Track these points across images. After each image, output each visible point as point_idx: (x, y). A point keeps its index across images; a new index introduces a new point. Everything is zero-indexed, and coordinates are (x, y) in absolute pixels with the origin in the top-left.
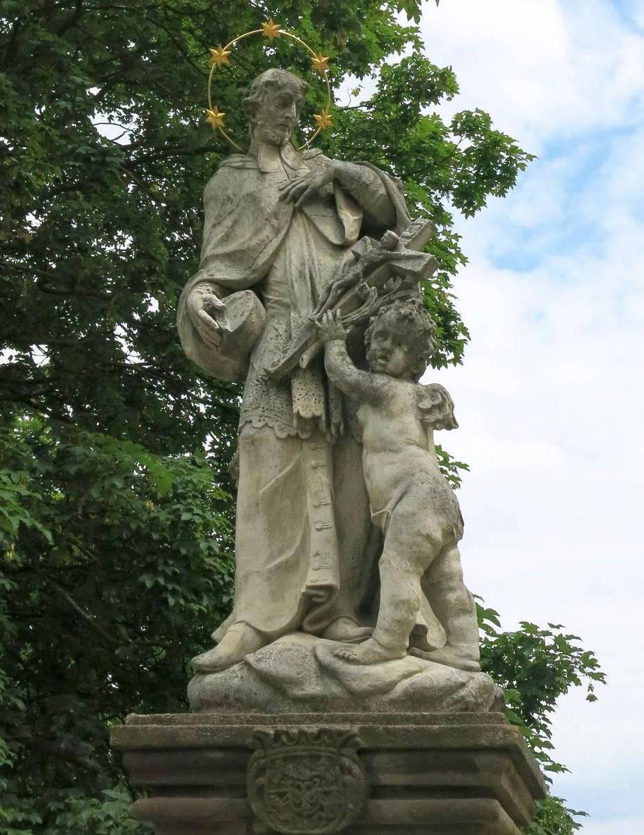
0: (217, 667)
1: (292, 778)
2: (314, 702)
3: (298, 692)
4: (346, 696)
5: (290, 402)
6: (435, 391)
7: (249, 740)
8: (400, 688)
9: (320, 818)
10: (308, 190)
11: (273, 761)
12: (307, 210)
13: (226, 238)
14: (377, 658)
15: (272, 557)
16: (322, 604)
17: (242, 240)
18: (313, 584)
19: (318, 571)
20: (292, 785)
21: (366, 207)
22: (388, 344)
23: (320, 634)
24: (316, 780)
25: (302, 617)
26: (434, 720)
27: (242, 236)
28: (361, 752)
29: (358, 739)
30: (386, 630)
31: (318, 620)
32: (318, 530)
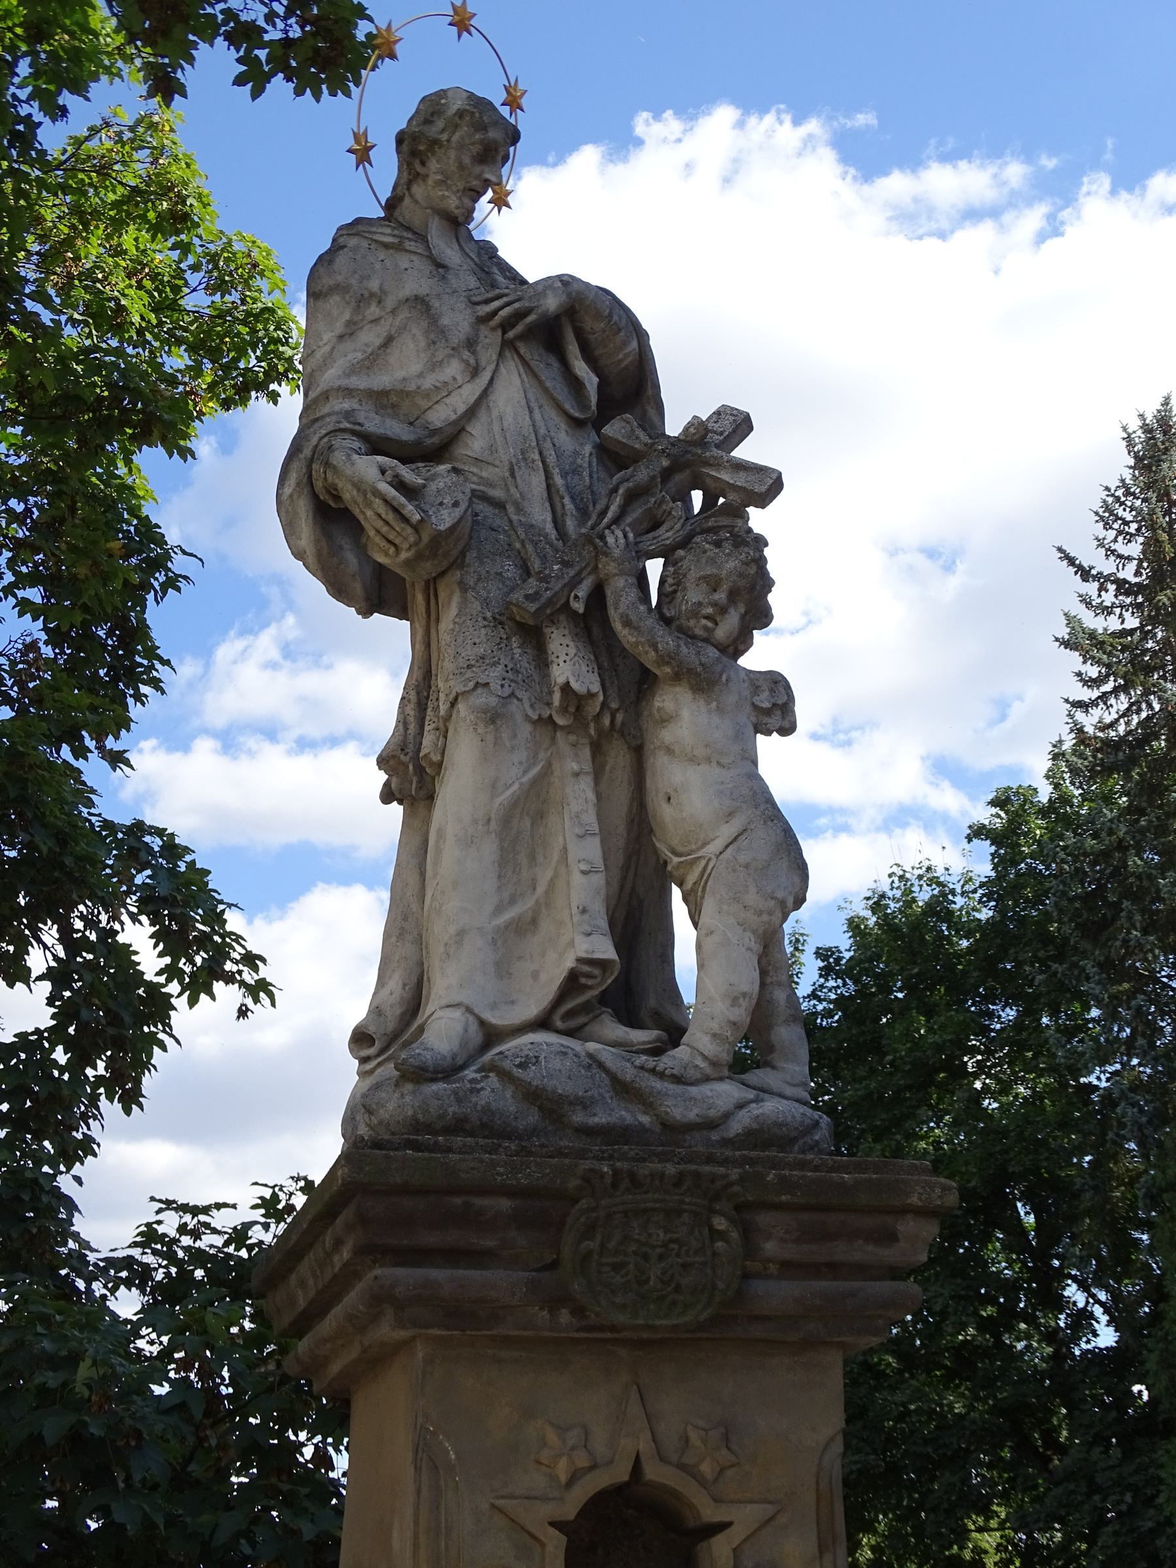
0: (438, 1072)
1: (638, 1241)
3: (578, 1117)
5: (542, 661)
8: (736, 1127)
10: (531, 318)
13: (372, 361)
14: (699, 1076)
15: (499, 909)
16: (590, 988)
17: (400, 374)
18: (590, 956)
19: (591, 938)
20: (635, 1253)
23: (570, 1033)
24: (672, 1246)
30: (714, 1035)
32: (584, 873)
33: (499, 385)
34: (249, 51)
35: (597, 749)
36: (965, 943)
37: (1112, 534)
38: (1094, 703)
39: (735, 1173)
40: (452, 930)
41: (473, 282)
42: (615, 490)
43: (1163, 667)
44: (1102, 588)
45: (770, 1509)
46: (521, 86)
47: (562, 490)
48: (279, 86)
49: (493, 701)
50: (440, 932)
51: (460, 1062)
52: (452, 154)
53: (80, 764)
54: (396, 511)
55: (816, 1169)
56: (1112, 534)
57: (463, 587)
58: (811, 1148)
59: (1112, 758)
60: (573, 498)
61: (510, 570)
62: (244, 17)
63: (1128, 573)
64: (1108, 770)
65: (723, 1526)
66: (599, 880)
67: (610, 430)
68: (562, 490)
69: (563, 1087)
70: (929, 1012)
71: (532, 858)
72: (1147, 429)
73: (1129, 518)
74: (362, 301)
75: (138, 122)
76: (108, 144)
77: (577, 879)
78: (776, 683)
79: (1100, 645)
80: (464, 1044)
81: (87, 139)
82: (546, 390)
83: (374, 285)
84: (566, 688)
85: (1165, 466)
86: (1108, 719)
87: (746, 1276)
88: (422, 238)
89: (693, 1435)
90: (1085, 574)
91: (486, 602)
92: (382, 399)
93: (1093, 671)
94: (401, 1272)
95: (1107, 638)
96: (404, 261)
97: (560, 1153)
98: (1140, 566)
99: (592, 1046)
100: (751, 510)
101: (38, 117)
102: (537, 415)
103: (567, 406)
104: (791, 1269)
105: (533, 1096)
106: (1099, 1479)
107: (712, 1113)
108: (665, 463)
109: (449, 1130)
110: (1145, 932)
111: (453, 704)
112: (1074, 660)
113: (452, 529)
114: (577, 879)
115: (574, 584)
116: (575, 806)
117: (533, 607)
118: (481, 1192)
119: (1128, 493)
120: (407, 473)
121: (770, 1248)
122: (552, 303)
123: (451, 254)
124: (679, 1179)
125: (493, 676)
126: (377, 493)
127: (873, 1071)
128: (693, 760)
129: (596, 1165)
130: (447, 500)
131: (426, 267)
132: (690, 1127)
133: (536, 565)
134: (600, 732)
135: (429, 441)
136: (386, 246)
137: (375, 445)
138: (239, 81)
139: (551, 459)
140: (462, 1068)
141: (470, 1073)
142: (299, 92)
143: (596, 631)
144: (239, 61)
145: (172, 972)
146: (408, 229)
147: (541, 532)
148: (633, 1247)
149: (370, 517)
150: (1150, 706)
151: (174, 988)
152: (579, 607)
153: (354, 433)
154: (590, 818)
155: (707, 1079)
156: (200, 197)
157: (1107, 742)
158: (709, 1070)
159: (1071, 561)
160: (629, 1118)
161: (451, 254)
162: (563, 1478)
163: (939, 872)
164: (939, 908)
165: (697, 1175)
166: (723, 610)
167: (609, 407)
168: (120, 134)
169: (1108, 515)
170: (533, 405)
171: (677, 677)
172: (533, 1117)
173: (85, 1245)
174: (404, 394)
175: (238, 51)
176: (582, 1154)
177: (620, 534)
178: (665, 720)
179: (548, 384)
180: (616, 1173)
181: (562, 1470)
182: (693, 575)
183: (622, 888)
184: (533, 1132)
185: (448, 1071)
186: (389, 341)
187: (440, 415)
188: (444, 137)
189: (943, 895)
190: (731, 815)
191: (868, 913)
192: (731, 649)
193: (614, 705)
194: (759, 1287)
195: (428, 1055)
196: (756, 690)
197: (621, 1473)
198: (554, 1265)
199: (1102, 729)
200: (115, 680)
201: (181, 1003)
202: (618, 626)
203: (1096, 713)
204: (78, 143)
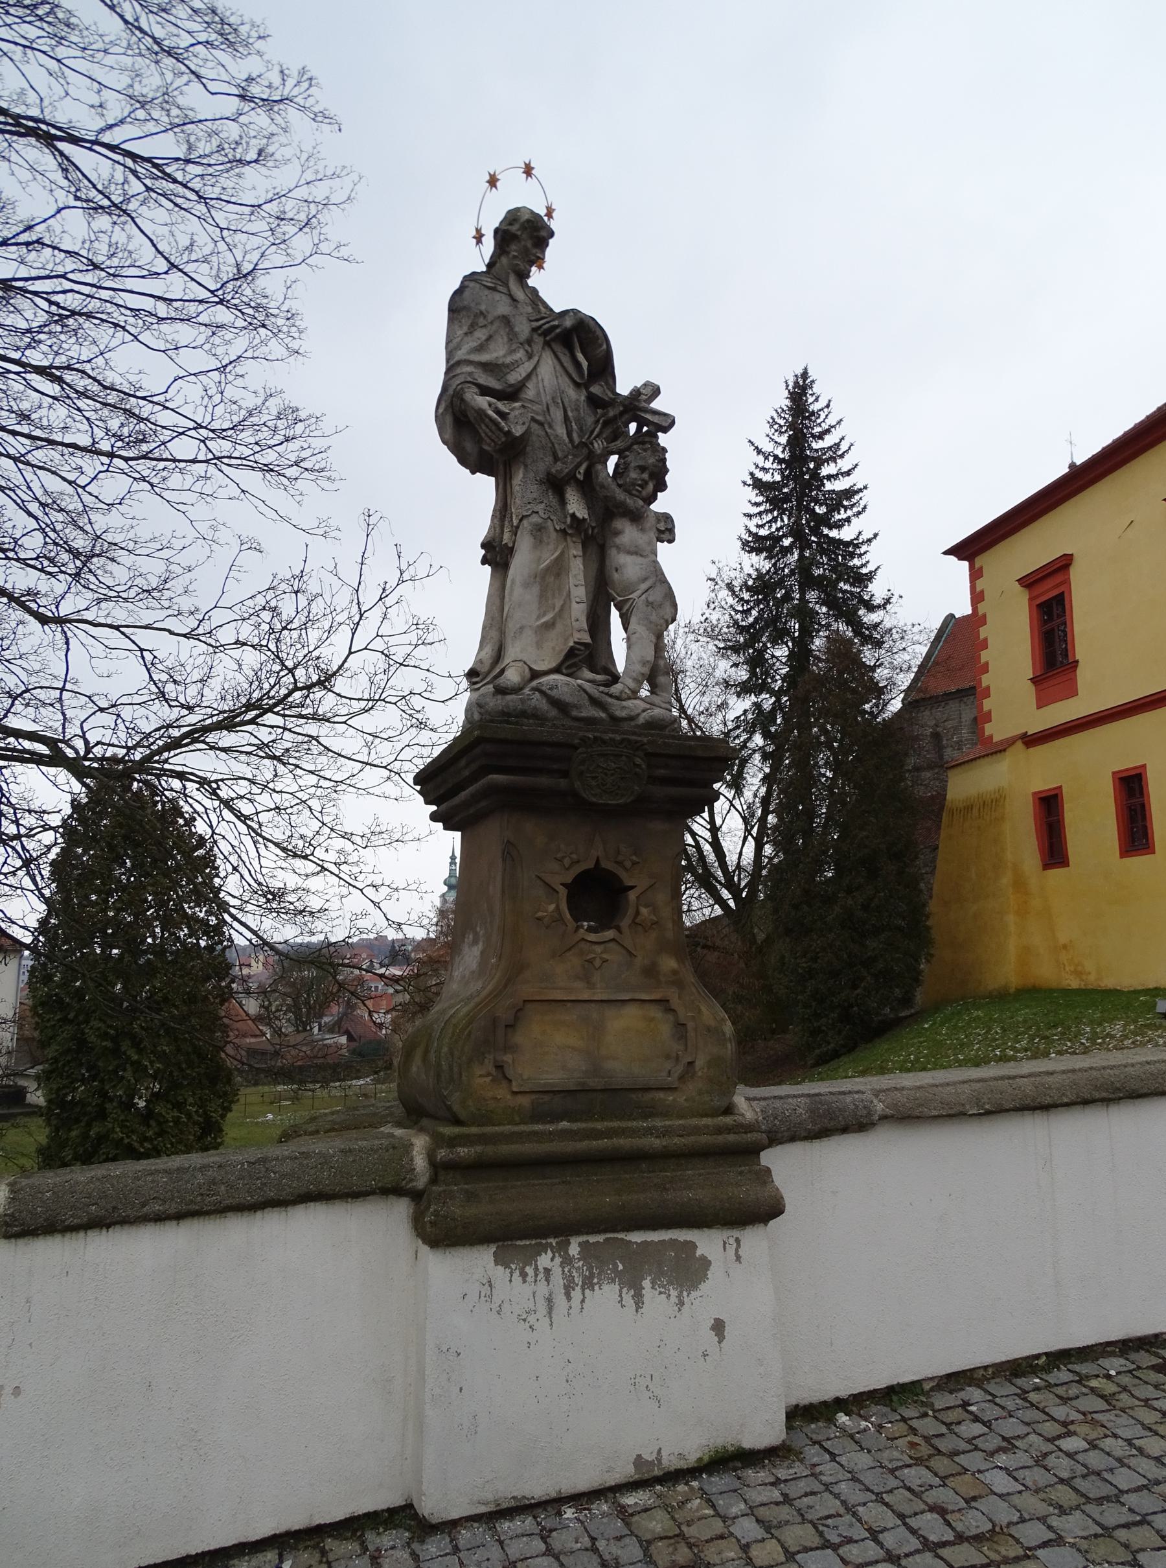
2: (590, 721)
3: (575, 713)
4: (608, 719)
5: (563, 502)
6: (667, 518)
7: (577, 741)
8: (641, 720)
9: (617, 794)
10: (558, 331)
12: (554, 345)
13: (480, 348)
15: (538, 618)
17: (495, 355)
22: (645, 476)
25: (563, 662)
27: (495, 351)
28: (648, 755)
29: (646, 747)
32: (578, 603)
33: (542, 362)
38: (755, 515)
40: (518, 626)
41: (529, 309)
50: (512, 626)
63: (778, 452)
69: (568, 699)
78: (667, 518)
84: (573, 516)
96: (497, 296)
98: (784, 449)
114: (574, 605)
120: (500, 405)
123: (519, 294)
136: (489, 288)
150: (782, 520)
152: (580, 477)
155: (629, 698)
165: (629, 741)
169: (773, 423)
182: (633, 465)
187: (514, 377)
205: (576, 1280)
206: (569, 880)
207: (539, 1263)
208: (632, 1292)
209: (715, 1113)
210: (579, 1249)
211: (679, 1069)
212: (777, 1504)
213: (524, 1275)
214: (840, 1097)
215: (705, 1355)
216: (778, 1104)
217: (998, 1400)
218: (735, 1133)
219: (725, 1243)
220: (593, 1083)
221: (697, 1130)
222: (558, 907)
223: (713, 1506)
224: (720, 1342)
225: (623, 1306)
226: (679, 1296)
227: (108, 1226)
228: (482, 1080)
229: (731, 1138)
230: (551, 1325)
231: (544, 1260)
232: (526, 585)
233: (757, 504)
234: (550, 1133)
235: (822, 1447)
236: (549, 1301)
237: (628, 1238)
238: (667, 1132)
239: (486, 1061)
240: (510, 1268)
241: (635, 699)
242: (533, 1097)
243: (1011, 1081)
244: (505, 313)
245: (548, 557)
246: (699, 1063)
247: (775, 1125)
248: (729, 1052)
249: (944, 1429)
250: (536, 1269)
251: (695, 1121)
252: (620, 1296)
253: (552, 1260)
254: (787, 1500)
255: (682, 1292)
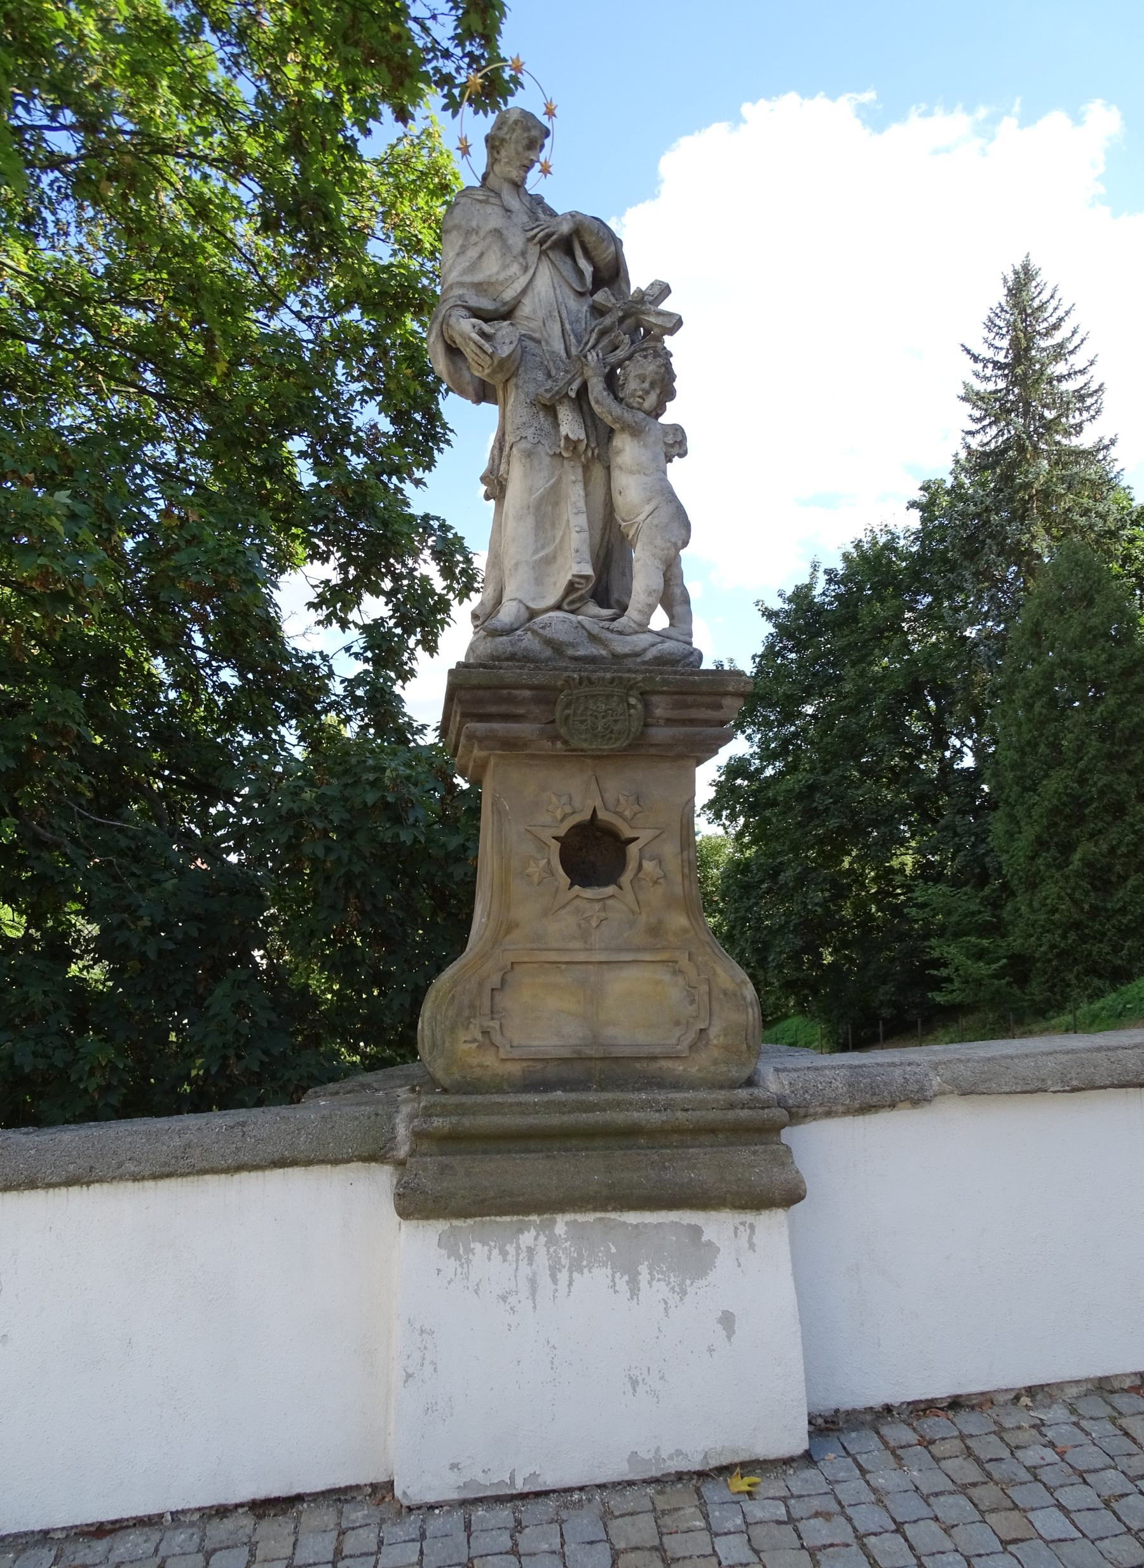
3: (570, 652)
5: (556, 424)
8: (649, 655)
11: (578, 698)
13: (473, 267)
15: (536, 552)
17: (488, 273)
21: (597, 259)
23: (572, 612)
26: (676, 673)
31: (572, 602)
33: (538, 275)
34: (449, 90)
35: (586, 468)
36: (904, 564)
37: (992, 335)
38: (978, 432)
39: (640, 677)
40: (513, 562)
41: (525, 219)
42: (593, 330)
43: (1017, 410)
44: (985, 366)
45: (658, 832)
46: (554, 103)
47: (570, 332)
48: (467, 110)
49: (529, 446)
50: (508, 564)
51: (515, 626)
52: (512, 146)
53: (402, 486)
54: (481, 348)
55: (682, 674)
56: (992, 335)
57: (517, 387)
58: (688, 665)
59: (986, 462)
60: (576, 336)
61: (540, 376)
62: (444, 71)
63: (1001, 358)
64: (984, 468)
65: (635, 839)
66: (586, 535)
67: (597, 297)
68: (570, 332)
69: (562, 637)
70: (882, 600)
71: (553, 525)
72: (1016, 273)
73: (1002, 324)
74: (468, 233)
75: (422, 133)
76: (408, 147)
77: (574, 535)
78: (677, 430)
79: (982, 399)
80: (517, 617)
81: (397, 145)
82: (563, 277)
83: (474, 224)
84: (567, 437)
85: (1024, 294)
86: (985, 441)
87: (646, 725)
88: (498, 195)
89: (622, 799)
90: (976, 359)
91: (527, 395)
92: (479, 288)
93: (977, 414)
94: (479, 725)
95: (987, 395)
96: (489, 209)
97: (555, 669)
98: (1007, 352)
99: (580, 618)
100: (666, 338)
101: (357, 135)
102: (558, 291)
103: (574, 285)
104: (670, 722)
105: (548, 642)
106: (959, 830)
107: (637, 649)
108: (620, 314)
109: (507, 659)
110: (998, 556)
111: (511, 448)
112: (967, 407)
113: (510, 356)
114: (574, 535)
115: (570, 383)
116: (573, 499)
117: (548, 396)
118: (517, 688)
119: (1002, 310)
120: (486, 328)
121: (658, 712)
122: (565, 228)
123: (514, 203)
124: (612, 680)
125: (529, 433)
126: (470, 339)
127: (852, 632)
128: (632, 472)
129: (571, 674)
130: (507, 341)
131: (498, 211)
132: (626, 656)
133: (553, 372)
134: (588, 460)
135: (502, 309)
136: (480, 201)
137: (476, 313)
138: (445, 108)
139: (564, 315)
140: (517, 629)
141: (519, 632)
142: (476, 113)
143: (585, 407)
144: (444, 96)
145: (449, 588)
146: (492, 191)
147: (558, 356)
148: (589, 713)
149: (469, 351)
150: (1009, 432)
151: (451, 596)
152: (573, 394)
153: (463, 307)
154: (581, 504)
155: (636, 633)
156: (454, 174)
157: (984, 453)
158: (637, 628)
159: (968, 352)
160: (595, 652)
161: (514, 203)
162: (559, 818)
163: (891, 527)
164: (890, 546)
165: (620, 678)
166: (647, 393)
167: (599, 282)
168: (412, 141)
169: (991, 325)
170: (556, 285)
171: (623, 429)
172: (548, 652)
173: (410, 718)
174: (490, 284)
175: (442, 90)
176: (566, 669)
177: (594, 354)
178: (619, 452)
179: (565, 273)
180: (581, 678)
181: (559, 815)
182: (632, 374)
183: (602, 539)
184: (549, 659)
185: (509, 631)
186: (482, 255)
187: (509, 294)
188: (507, 137)
189: (893, 539)
190: (649, 500)
191: (853, 550)
192: (654, 413)
193: (593, 445)
194: (653, 731)
195: (498, 624)
196: (666, 434)
197: (587, 816)
198: (553, 721)
199: (982, 446)
200: (427, 441)
201: (455, 603)
202: (593, 403)
203: (979, 437)
204: (393, 147)
205: (563, 1261)
206: (562, 832)
207: (521, 1242)
208: (626, 1278)
209: (733, 1085)
210: (565, 1228)
211: (691, 1036)
212: (779, 1523)
213: (504, 1254)
214: (888, 1069)
215: (711, 1350)
216: (811, 1075)
217: (1083, 1423)
218: (750, 1108)
219: (736, 1228)
220: (589, 1052)
221: (702, 1105)
222: (549, 862)
223: (706, 1517)
224: (729, 1337)
225: (616, 1292)
226: (682, 1284)
227: (88, 1184)
228: (466, 1046)
229: (744, 1114)
230: (535, 1307)
231: (527, 1238)
232: (519, 518)
233: (980, 420)
234: (535, 1104)
235: (855, 1461)
236: (533, 1282)
237: (622, 1219)
238: (668, 1106)
239: (472, 1026)
240: (489, 1245)
241: (644, 632)
242: (524, 1064)
243: (1109, 1053)
244: (497, 226)
245: (542, 484)
246: (713, 1032)
247: (805, 1099)
248: (751, 1018)
249: (1006, 1454)
250: (518, 1248)
251: (703, 1095)
252: (613, 1281)
253: (536, 1239)
254: (791, 1520)
255: (684, 1280)
